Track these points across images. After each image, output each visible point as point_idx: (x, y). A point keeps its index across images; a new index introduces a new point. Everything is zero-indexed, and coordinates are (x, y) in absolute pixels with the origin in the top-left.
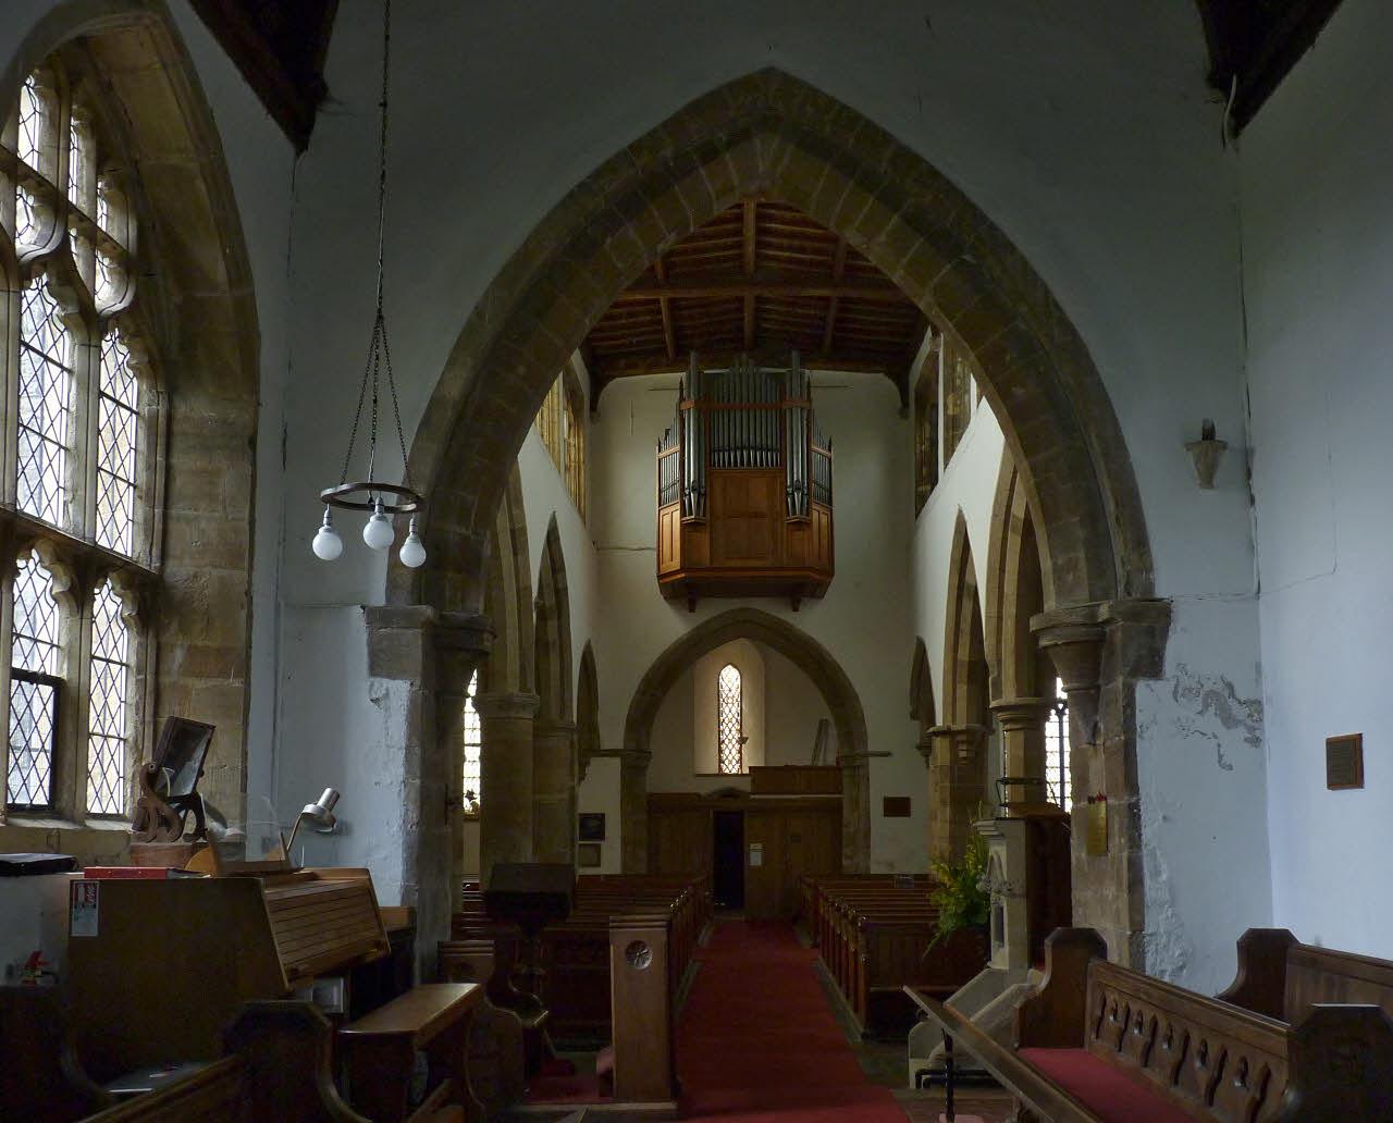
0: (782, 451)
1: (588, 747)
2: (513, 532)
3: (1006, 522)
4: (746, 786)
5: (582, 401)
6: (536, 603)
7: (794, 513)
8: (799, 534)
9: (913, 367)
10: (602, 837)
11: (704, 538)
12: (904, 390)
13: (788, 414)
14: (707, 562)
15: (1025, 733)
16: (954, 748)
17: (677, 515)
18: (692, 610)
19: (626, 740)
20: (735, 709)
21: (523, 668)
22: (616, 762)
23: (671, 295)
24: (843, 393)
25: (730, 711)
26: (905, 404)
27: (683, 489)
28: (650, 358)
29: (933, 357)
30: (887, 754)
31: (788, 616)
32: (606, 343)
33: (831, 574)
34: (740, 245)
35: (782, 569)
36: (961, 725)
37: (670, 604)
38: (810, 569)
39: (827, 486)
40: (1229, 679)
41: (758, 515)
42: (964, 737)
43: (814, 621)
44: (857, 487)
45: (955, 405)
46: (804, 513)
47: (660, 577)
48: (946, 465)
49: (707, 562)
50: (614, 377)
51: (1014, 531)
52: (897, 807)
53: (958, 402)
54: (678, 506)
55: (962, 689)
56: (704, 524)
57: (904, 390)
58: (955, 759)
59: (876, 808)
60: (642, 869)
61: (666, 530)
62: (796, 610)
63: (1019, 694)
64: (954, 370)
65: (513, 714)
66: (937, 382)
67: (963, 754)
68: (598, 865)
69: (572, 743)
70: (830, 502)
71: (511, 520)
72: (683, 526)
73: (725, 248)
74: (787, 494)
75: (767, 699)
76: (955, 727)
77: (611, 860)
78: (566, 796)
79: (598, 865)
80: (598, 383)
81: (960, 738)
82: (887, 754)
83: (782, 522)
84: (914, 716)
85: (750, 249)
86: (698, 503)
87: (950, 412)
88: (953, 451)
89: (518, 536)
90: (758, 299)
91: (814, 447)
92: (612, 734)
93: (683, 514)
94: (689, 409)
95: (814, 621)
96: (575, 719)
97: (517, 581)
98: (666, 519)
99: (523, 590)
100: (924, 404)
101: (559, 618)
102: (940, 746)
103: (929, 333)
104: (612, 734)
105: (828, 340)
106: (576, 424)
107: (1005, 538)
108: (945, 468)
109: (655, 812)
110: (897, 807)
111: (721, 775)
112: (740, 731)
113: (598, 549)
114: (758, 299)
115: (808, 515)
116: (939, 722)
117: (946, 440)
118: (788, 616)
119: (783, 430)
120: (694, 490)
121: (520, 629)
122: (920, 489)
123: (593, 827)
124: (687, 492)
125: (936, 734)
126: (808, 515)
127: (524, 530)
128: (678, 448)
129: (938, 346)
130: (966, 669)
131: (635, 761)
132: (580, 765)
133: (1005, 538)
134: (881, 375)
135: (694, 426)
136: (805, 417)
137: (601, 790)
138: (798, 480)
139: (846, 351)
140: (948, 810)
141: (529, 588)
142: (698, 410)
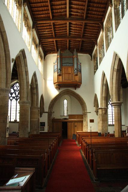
0: (73, 64)
1: (42, 111)
2: (26, 71)
3: (113, 70)
4: (68, 117)
6: (30, 85)
8: (76, 77)
10: (45, 126)
11: (61, 77)
12: (91, 56)
14: (61, 81)
15: (118, 108)
16: (102, 111)
17: (57, 74)
19: (48, 110)
20: (66, 106)
21: (27, 96)
22: (47, 114)
23: (54, 22)
24: (83, 58)
25: (65, 106)
26: (92, 59)
28: (53, 51)
29: (97, 49)
30: (90, 113)
33: (81, 83)
34: (66, 32)
35: (73, 82)
36: (103, 107)
40: (96, 113)
41: (70, 74)
42: (104, 109)
43: (78, 91)
44: (85, 69)
47: (54, 84)
48: (116, 30)
49: (61, 81)
51: (115, 71)
52: (92, 121)
54: (57, 72)
55: (103, 101)
57: (91, 56)
58: (102, 113)
59: (89, 121)
60: (51, 131)
62: (75, 89)
63: (116, 101)
64: (100, 50)
65: (25, 104)
66: (97, 54)
67: (104, 112)
68: (44, 130)
69: (39, 111)
71: (25, 69)
72: (58, 75)
73: (64, 32)
75: (70, 104)
76: (102, 108)
77: (46, 129)
78: (37, 119)
79: (44, 130)
80: (45, 55)
81: (103, 109)
82: (90, 113)
84: (94, 106)
85: (68, 32)
89: (27, 72)
91: (78, 63)
92: (46, 109)
95: (78, 91)
96: (39, 107)
97: (27, 80)
98: (55, 74)
99: (28, 82)
100: (95, 58)
101: (37, 89)
102: (100, 111)
103: (96, 46)
104: (46, 109)
105: (80, 49)
107: (113, 73)
109: (53, 121)
110: (92, 121)
111: (64, 116)
112: (67, 109)
116: (100, 107)
119: (73, 60)
121: (27, 89)
123: (43, 124)
125: (99, 109)
127: (38, 84)
129: (97, 47)
130: (104, 98)
131: (50, 114)
132: (40, 114)
133: (113, 73)
137: (44, 118)
139: (83, 51)
140: (101, 121)
141: (29, 82)
142: (60, 57)
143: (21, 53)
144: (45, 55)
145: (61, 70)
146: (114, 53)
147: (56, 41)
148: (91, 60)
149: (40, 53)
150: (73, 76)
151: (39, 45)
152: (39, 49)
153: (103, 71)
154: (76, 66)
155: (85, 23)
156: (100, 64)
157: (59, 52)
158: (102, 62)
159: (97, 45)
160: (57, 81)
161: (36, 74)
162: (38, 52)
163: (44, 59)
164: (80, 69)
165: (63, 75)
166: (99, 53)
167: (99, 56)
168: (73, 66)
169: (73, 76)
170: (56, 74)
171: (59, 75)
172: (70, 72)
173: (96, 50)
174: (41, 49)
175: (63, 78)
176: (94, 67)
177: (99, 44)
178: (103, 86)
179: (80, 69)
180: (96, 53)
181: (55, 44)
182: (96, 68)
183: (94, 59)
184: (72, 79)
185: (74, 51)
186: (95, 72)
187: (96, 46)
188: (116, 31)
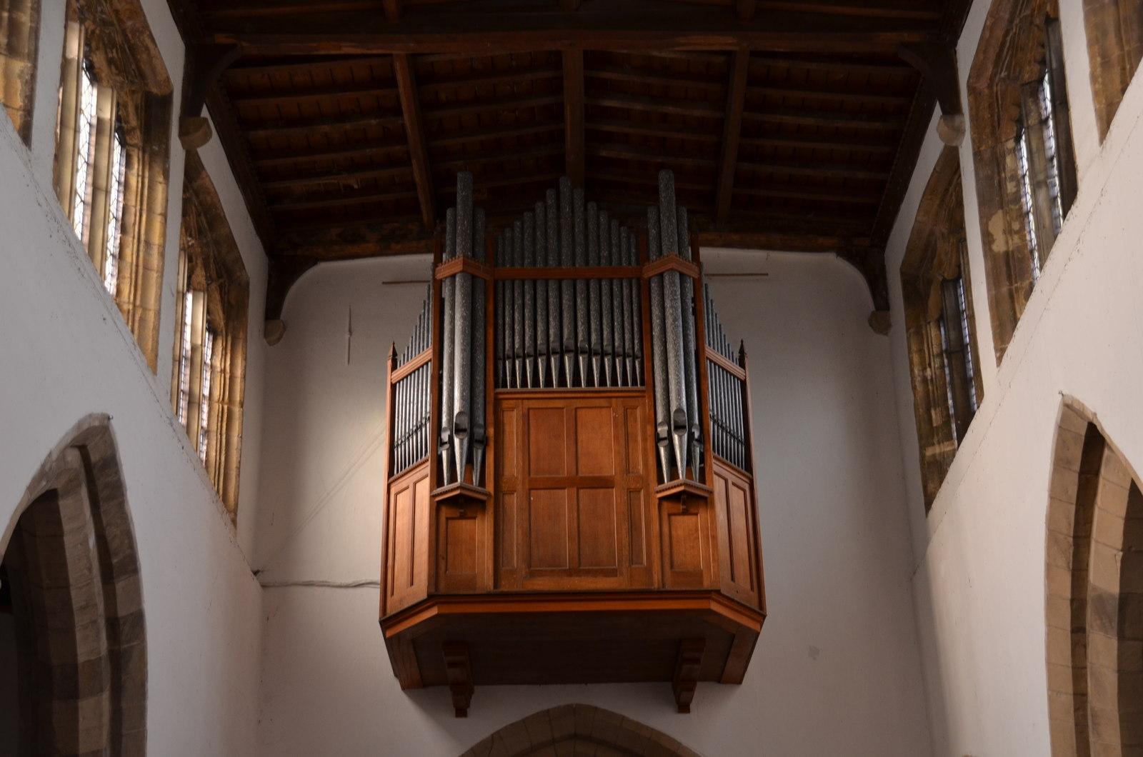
0: (645, 357)
5: (244, 288)
7: (673, 474)
8: (683, 524)
9: (896, 226)
11: (480, 530)
13: (654, 286)
18: (461, 712)
24: (771, 292)
27: (438, 429)
29: (950, 160)
31: (666, 723)
32: (298, 186)
37: (413, 698)
38: (714, 594)
39: (741, 432)
41: (603, 483)
45: (1009, 231)
46: (696, 475)
48: (1001, 351)
49: (486, 581)
50: (315, 260)
53: (1016, 226)
54: (427, 469)
56: (483, 503)
61: (402, 522)
62: (684, 708)
70: (749, 467)
72: (438, 506)
74: (658, 439)
80: (283, 272)
83: (648, 495)
86: (469, 460)
87: (999, 246)
88: (1015, 321)
90: (595, 60)
91: (710, 352)
93: (437, 480)
94: (453, 276)
98: (404, 501)
103: (938, 111)
106: (226, 324)
108: (999, 360)
113: (264, 586)
114: (595, 60)
115: (703, 480)
117: (995, 305)
118: (666, 723)
120: (459, 430)
122: (929, 452)
124: (445, 436)
126: (703, 480)
127: (138, 619)
128: (428, 354)
129: (959, 131)
134: (831, 258)
135: (463, 383)
136: (690, 295)
138: (679, 410)
143: (74, 457)
144: (283, 272)
145: (480, 430)
146: (1070, 410)
147: (423, 76)
148: (880, 318)
149: (200, 213)
150: (648, 511)
151: (190, 110)
152: (193, 169)
153: (1070, 410)
154: (676, 392)
155: (754, 54)
156: (1005, 326)
157: (459, 218)
158: (1031, 314)
159: (952, 109)
160: (420, 589)
161: (111, 463)
162: (169, 194)
163: (272, 311)
164: (735, 424)
165: (513, 502)
166: (982, 203)
167: (987, 239)
168: (645, 379)
169: (648, 511)
170: (419, 492)
171: (453, 507)
172: (609, 465)
173: (930, 189)
174: (213, 155)
175: (515, 535)
176: (930, 401)
177: (971, 89)
178: (1078, 630)
179: (735, 424)
180: (943, 228)
181: (408, 119)
182: (951, 403)
183: (908, 297)
184: (634, 557)
185: (652, 192)
186: (935, 471)
187: (938, 111)
188: (999, 360)
